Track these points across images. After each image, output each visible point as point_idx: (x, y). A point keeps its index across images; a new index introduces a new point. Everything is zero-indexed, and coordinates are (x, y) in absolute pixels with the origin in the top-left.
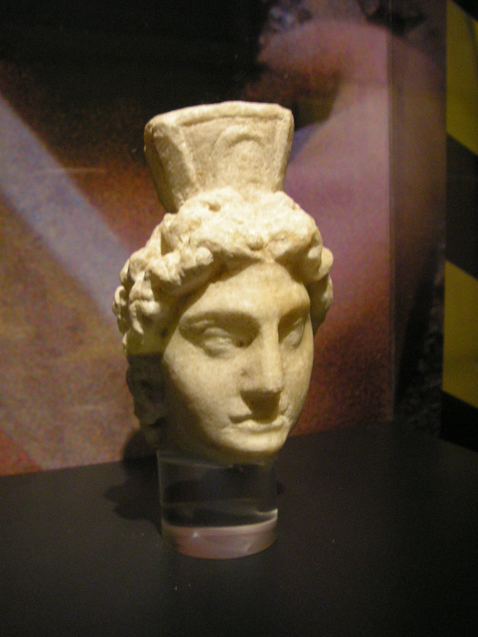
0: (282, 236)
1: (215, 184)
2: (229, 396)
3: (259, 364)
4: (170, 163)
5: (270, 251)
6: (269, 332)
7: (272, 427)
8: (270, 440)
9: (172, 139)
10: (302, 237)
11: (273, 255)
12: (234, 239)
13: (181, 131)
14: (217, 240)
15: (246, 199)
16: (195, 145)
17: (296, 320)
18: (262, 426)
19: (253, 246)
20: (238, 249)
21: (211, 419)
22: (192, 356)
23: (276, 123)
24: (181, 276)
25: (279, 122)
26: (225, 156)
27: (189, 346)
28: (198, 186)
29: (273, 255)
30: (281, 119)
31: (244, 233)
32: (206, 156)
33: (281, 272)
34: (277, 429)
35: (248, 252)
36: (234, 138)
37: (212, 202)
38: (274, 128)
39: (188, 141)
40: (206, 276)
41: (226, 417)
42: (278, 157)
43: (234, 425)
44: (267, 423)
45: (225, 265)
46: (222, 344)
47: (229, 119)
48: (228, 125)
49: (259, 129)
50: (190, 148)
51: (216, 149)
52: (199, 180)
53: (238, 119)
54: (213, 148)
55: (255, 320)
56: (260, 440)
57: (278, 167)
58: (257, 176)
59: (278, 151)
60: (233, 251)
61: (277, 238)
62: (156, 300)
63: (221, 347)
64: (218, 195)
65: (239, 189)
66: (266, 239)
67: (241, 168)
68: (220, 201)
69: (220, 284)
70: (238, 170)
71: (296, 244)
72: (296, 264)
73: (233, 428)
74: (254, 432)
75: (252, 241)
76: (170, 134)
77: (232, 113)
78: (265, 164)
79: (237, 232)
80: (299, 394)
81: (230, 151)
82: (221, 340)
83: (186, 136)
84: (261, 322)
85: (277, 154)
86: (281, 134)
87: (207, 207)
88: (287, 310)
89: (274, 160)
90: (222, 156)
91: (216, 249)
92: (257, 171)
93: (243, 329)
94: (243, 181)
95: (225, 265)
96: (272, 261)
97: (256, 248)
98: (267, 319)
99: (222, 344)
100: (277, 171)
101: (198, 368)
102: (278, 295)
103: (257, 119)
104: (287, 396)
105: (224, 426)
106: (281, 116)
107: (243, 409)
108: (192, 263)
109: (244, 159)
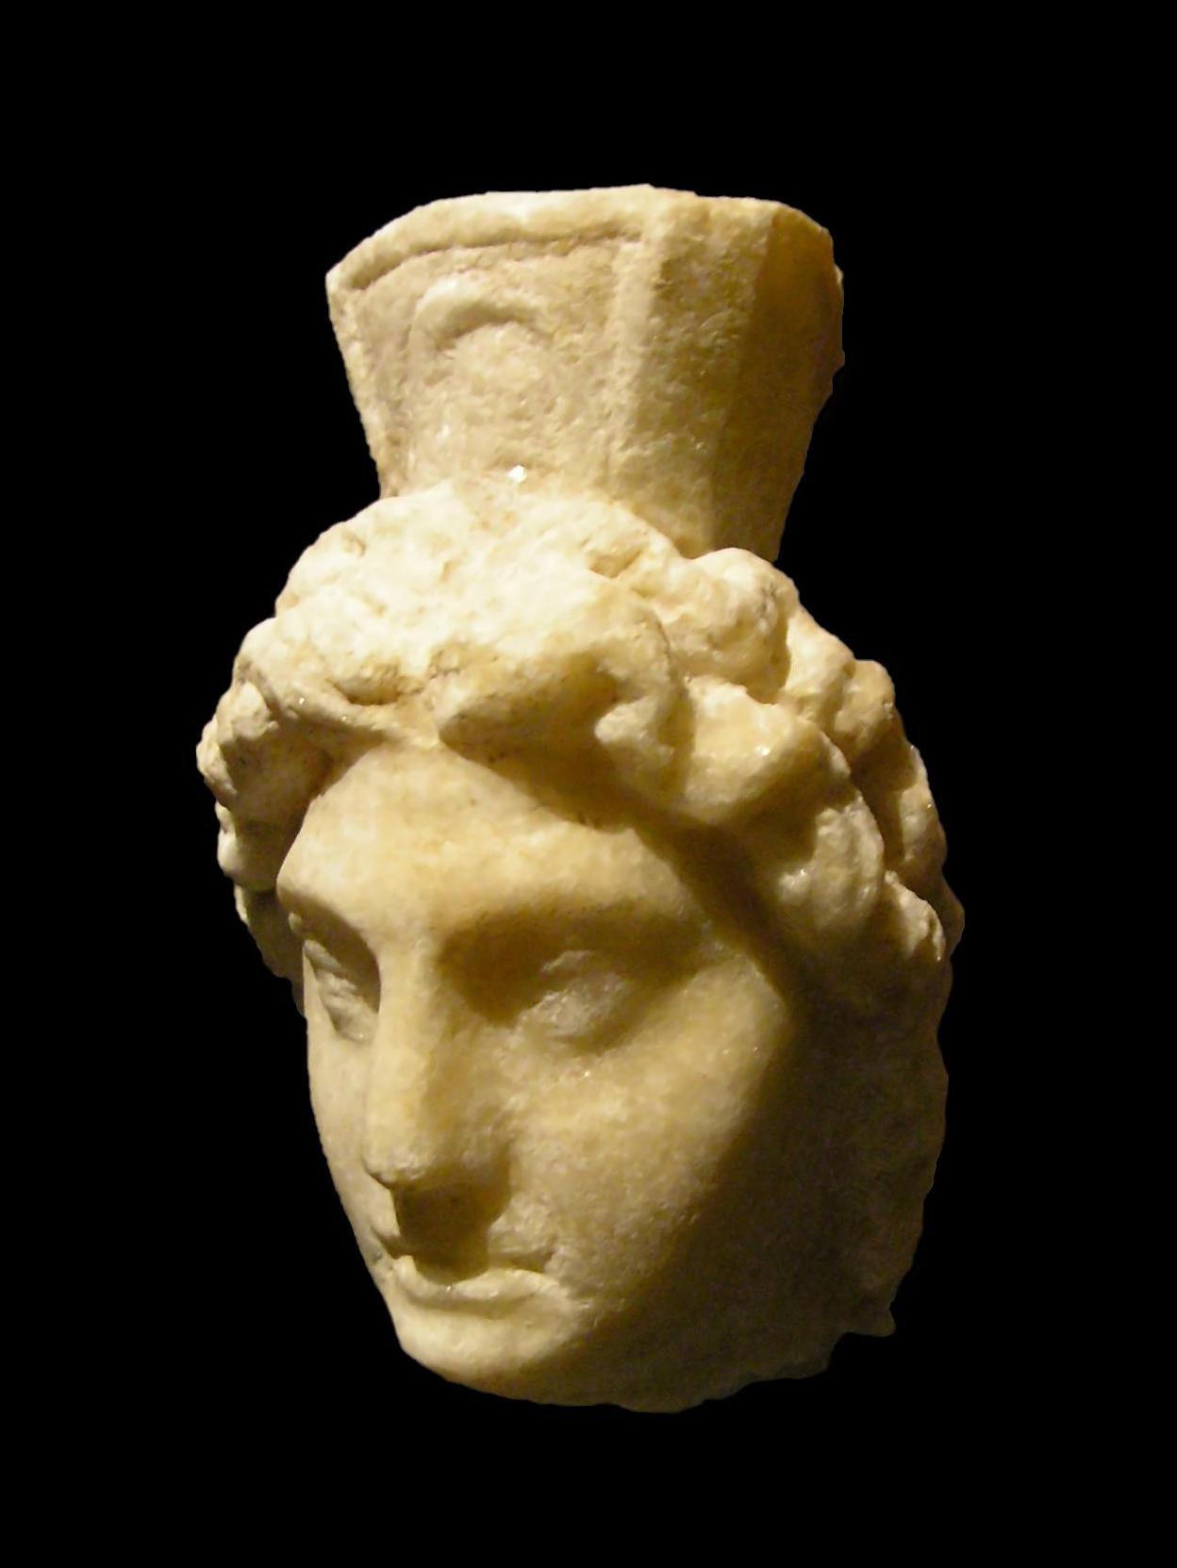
0: (454, 662)
12: (297, 661)
15: (485, 525)
23: (614, 252)
25: (626, 247)
26: (431, 382)
30: (635, 237)
33: (463, 778)
35: (339, 708)
38: (606, 270)
47: (433, 255)
48: (434, 278)
49: (524, 281)
53: (459, 254)
56: (441, 1332)
57: (621, 408)
58: (527, 448)
59: (619, 351)
61: (445, 664)
66: (416, 665)
67: (473, 420)
70: (464, 426)
75: (342, 671)
77: (435, 236)
78: (562, 403)
84: (372, 942)
85: (618, 363)
86: (628, 290)
88: (462, 912)
89: (601, 384)
90: (421, 385)
92: (525, 425)
95: (314, 751)
96: (435, 742)
97: (385, 691)
99: (336, 994)
100: (620, 424)
102: (432, 860)
103: (520, 247)
104: (544, 1211)
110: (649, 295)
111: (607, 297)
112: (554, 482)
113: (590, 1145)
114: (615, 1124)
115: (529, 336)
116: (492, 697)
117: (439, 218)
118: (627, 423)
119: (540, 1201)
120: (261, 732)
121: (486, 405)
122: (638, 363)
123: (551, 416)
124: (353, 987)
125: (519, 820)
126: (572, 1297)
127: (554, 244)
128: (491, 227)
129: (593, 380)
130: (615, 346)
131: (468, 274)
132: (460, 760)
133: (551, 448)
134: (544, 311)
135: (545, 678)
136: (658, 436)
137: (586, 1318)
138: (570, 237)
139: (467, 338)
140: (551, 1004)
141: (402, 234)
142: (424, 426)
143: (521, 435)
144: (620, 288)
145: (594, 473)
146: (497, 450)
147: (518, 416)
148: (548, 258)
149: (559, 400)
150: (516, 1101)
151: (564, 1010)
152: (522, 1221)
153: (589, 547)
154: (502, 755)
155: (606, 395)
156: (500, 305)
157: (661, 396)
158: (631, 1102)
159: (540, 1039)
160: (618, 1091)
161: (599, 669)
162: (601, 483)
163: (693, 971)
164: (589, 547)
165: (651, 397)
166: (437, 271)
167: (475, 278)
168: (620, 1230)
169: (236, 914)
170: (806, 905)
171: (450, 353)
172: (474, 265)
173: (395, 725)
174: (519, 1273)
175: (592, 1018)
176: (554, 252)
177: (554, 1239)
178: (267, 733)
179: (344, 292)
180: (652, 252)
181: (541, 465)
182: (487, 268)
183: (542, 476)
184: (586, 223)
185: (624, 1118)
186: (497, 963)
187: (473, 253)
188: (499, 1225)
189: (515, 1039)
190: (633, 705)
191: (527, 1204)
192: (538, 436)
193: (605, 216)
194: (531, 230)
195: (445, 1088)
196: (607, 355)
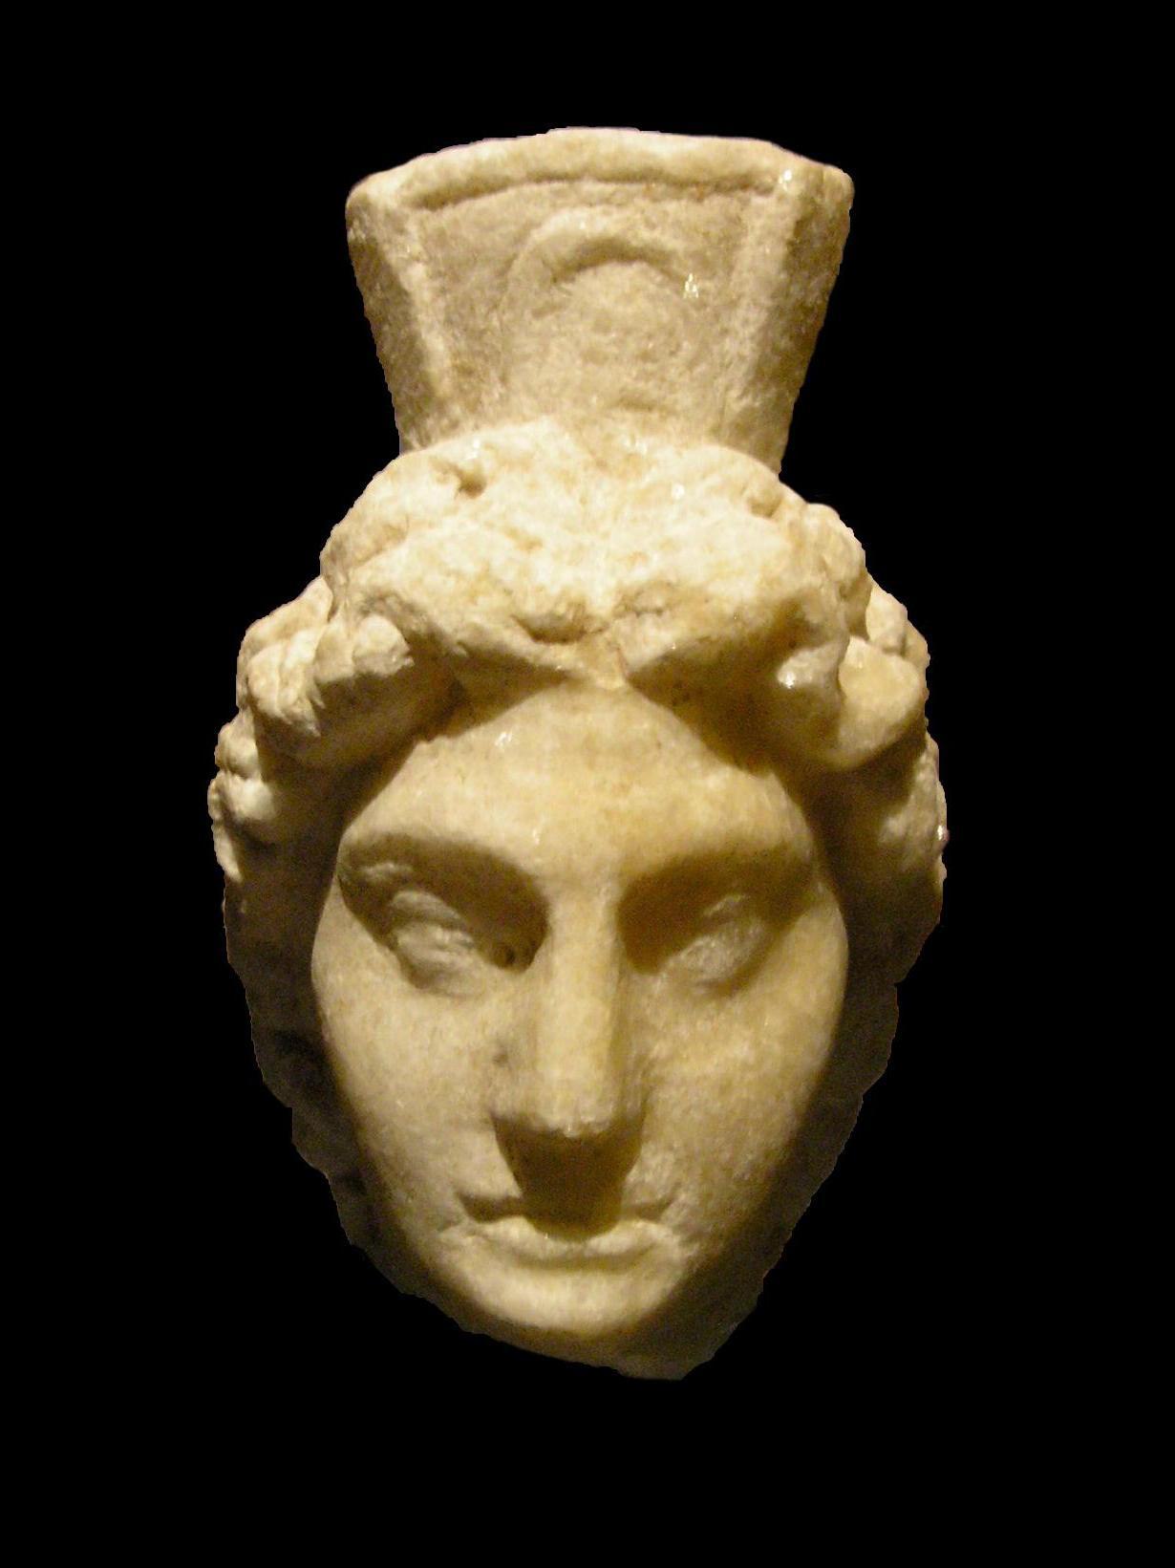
0: (659, 602)
1: (506, 410)
2: (457, 1124)
3: (531, 1029)
4: (386, 328)
5: (614, 647)
6: (582, 934)
7: (587, 1254)
8: (582, 1299)
9: (386, 247)
10: (729, 609)
11: (622, 662)
12: (472, 598)
13: (412, 227)
14: (420, 598)
15: (601, 465)
16: (449, 274)
17: (710, 902)
18: (550, 1245)
19: (536, 625)
20: (479, 631)
21: (410, 1193)
22: (368, 975)
23: (745, 203)
24: (315, 707)
25: (757, 201)
26: (538, 314)
27: (362, 940)
28: (456, 410)
29: (622, 662)
30: (766, 191)
31: (509, 577)
32: (482, 309)
33: (649, 721)
34: (611, 1264)
35: (519, 643)
36: (566, 251)
37: (466, 465)
38: (736, 221)
39: (431, 260)
40: (401, 713)
41: (450, 1192)
42: (746, 322)
43: (477, 1226)
44: (569, 1236)
45: (453, 686)
46: (442, 948)
47: (557, 185)
48: (554, 207)
49: (666, 224)
50: (437, 284)
51: (511, 286)
52: (459, 388)
53: (589, 187)
54: (503, 287)
55: (530, 878)
56: (540, 1289)
57: (742, 358)
58: (651, 390)
59: (745, 302)
60: (463, 636)
61: (641, 603)
62: (266, 779)
63: (443, 957)
64: (488, 446)
65: (579, 426)
66: (601, 602)
68: (488, 467)
69: (442, 742)
70: (579, 362)
71: (702, 631)
72: (728, 694)
73: (473, 1233)
74: (525, 1261)
75: (530, 607)
76: (381, 233)
78: (688, 347)
79: (486, 574)
80: (726, 1155)
81: (557, 297)
82: (440, 935)
83: (425, 241)
84: (549, 890)
85: (741, 312)
87: (455, 483)
88: (654, 856)
89: (725, 332)
90: (528, 315)
91: (415, 624)
92: (650, 367)
93: (504, 911)
94: (594, 400)
95: (453, 686)
96: (619, 683)
97: (565, 629)
98: (573, 882)
99: (442, 948)
100: (740, 373)
101: (377, 1019)
102: (623, 804)
103: (659, 188)
104: (671, 1157)
105: (448, 1224)
106: (768, 180)
107: (497, 1179)
108: (342, 668)
109: (602, 325)
110: (782, 251)
111: (736, 247)
112: (673, 425)
113: (725, 1088)
114: (746, 1067)
115: (659, 278)
116: (702, 640)
117: (569, 146)
118: (746, 374)
119: (671, 1148)
120: (394, 669)
121: (614, 342)
122: (764, 316)
123: (674, 360)
124: (469, 939)
125: (696, 764)
126: (684, 1244)
127: (694, 189)
128: (636, 165)
129: (718, 328)
130: (740, 296)
131: (599, 209)
132: (646, 703)
133: (672, 392)
134: (681, 254)
135: (760, 622)
136: (767, 388)
137: (690, 1262)
138: (706, 184)
139: (590, 272)
140: (699, 949)
141: (517, 158)
142: (526, 358)
143: (647, 376)
144: (750, 239)
145: (711, 421)
146: (622, 390)
147: (645, 356)
148: (684, 202)
149: (685, 344)
150: (659, 1049)
151: (711, 954)
152: (652, 1170)
153: (747, 493)
154: (687, 698)
155: (729, 345)
156: (634, 243)
157: (775, 350)
158: (756, 1044)
159: (683, 987)
160: (747, 1033)
161: (798, 615)
162: (716, 432)
163: (799, 912)
164: (747, 493)
165: (768, 350)
166: (560, 202)
167: (606, 213)
168: (737, 1173)
169: (220, 871)
170: (898, 849)
171: (565, 286)
172: (606, 200)
173: (581, 665)
174: (640, 1224)
175: (737, 961)
176: (692, 196)
177: (678, 1185)
178: (403, 670)
179: (407, 210)
180: (786, 208)
181: (662, 408)
182: (620, 205)
183: (663, 419)
184: (726, 172)
185: (752, 1060)
186: (663, 908)
187: (610, 188)
188: (633, 1176)
189: (659, 984)
190: (817, 651)
191: (655, 1154)
192: (663, 380)
193: (743, 167)
194: (674, 172)
195: (624, 1032)
196: (733, 304)
